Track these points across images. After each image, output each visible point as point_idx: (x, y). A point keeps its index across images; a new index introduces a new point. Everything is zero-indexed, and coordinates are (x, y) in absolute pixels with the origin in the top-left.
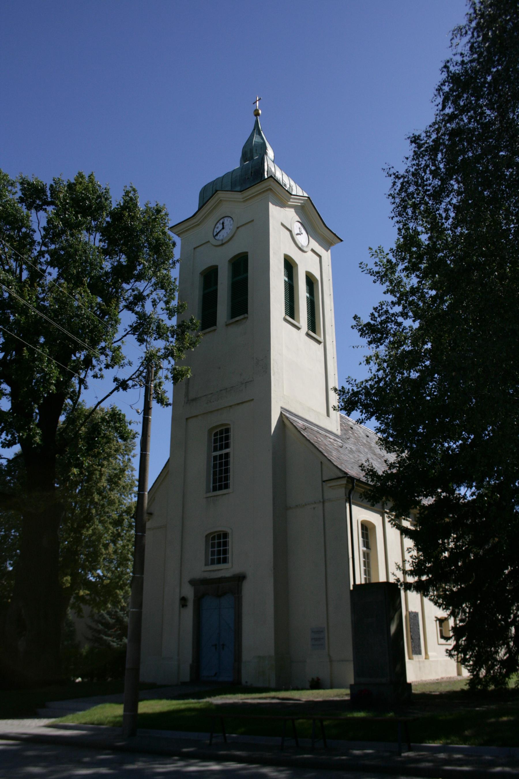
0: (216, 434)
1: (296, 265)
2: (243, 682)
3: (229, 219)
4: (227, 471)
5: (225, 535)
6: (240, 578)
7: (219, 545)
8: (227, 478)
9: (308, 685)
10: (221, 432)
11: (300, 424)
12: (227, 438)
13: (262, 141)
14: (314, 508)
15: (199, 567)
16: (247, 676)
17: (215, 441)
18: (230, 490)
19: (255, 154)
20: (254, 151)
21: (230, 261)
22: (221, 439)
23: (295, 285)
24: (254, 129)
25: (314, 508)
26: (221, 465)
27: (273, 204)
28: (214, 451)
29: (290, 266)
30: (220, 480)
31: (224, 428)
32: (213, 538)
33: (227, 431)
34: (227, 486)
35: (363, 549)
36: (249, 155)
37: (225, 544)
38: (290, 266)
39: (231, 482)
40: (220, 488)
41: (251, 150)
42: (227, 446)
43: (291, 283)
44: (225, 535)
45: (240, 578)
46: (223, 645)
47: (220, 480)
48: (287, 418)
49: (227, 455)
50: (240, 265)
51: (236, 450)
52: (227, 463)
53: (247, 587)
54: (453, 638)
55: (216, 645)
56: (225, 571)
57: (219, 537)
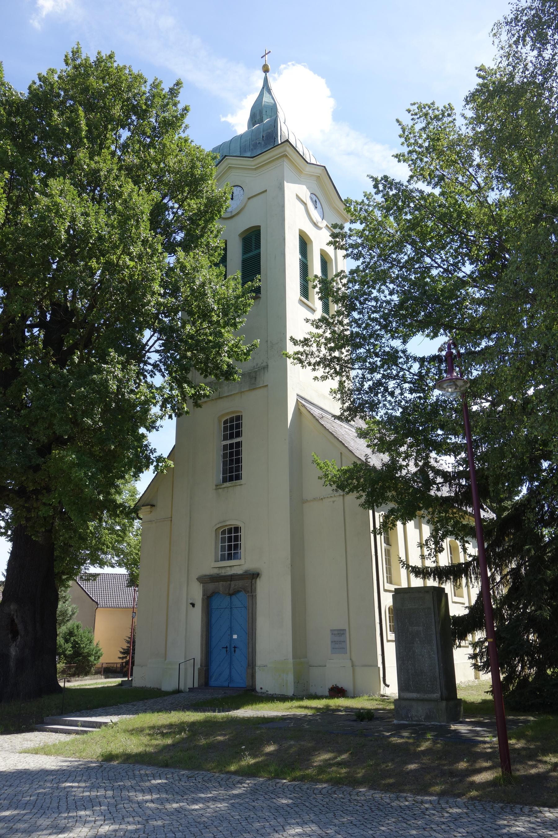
0: (226, 422)
1: (311, 242)
2: (258, 689)
3: (239, 189)
4: (239, 461)
5: (237, 529)
6: (253, 576)
7: (231, 541)
8: (239, 469)
9: (327, 693)
10: (232, 420)
11: (316, 412)
12: (239, 426)
13: (273, 101)
14: (334, 502)
15: (208, 562)
16: (264, 681)
17: (225, 429)
18: (242, 482)
19: (264, 116)
20: (264, 112)
21: (240, 235)
22: (232, 427)
23: (309, 264)
24: (263, 88)
25: (334, 502)
26: (231, 454)
27: (287, 182)
28: (224, 440)
29: (304, 244)
30: (231, 471)
31: (234, 415)
32: (223, 532)
33: (239, 418)
34: (238, 477)
35: (384, 545)
36: (258, 118)
37: (237, 538)
38: (304, 244)
39: (244, 472)
40: (231, 479)
41: (261, 113)
42: (238, 434)
43: (304, 260)
44: (237, 529)
45: (253, 576)
46: (235, 647)
47: (231, 471)
48: (304, 406)
49: (239, 444)
50: (252, 239)
51: (248, 439)
52: (238, 453)
53: (261, 586)
54: (405, 183)
55: (227, 647)
56: (236, 567)
57: (230, 531)
